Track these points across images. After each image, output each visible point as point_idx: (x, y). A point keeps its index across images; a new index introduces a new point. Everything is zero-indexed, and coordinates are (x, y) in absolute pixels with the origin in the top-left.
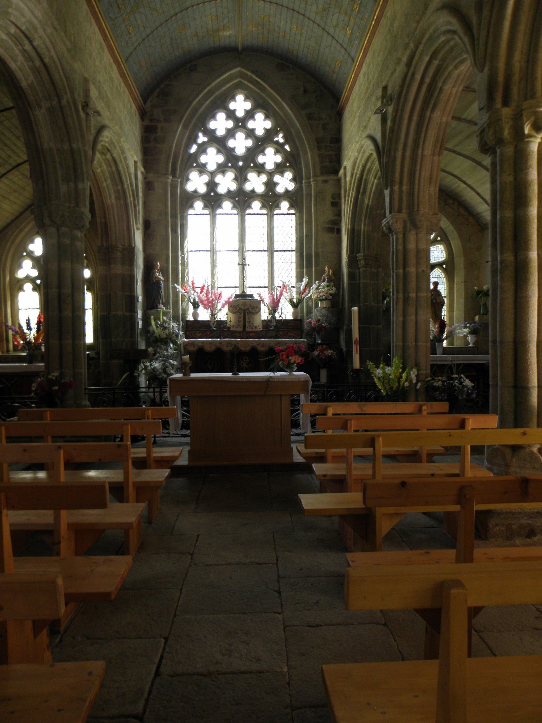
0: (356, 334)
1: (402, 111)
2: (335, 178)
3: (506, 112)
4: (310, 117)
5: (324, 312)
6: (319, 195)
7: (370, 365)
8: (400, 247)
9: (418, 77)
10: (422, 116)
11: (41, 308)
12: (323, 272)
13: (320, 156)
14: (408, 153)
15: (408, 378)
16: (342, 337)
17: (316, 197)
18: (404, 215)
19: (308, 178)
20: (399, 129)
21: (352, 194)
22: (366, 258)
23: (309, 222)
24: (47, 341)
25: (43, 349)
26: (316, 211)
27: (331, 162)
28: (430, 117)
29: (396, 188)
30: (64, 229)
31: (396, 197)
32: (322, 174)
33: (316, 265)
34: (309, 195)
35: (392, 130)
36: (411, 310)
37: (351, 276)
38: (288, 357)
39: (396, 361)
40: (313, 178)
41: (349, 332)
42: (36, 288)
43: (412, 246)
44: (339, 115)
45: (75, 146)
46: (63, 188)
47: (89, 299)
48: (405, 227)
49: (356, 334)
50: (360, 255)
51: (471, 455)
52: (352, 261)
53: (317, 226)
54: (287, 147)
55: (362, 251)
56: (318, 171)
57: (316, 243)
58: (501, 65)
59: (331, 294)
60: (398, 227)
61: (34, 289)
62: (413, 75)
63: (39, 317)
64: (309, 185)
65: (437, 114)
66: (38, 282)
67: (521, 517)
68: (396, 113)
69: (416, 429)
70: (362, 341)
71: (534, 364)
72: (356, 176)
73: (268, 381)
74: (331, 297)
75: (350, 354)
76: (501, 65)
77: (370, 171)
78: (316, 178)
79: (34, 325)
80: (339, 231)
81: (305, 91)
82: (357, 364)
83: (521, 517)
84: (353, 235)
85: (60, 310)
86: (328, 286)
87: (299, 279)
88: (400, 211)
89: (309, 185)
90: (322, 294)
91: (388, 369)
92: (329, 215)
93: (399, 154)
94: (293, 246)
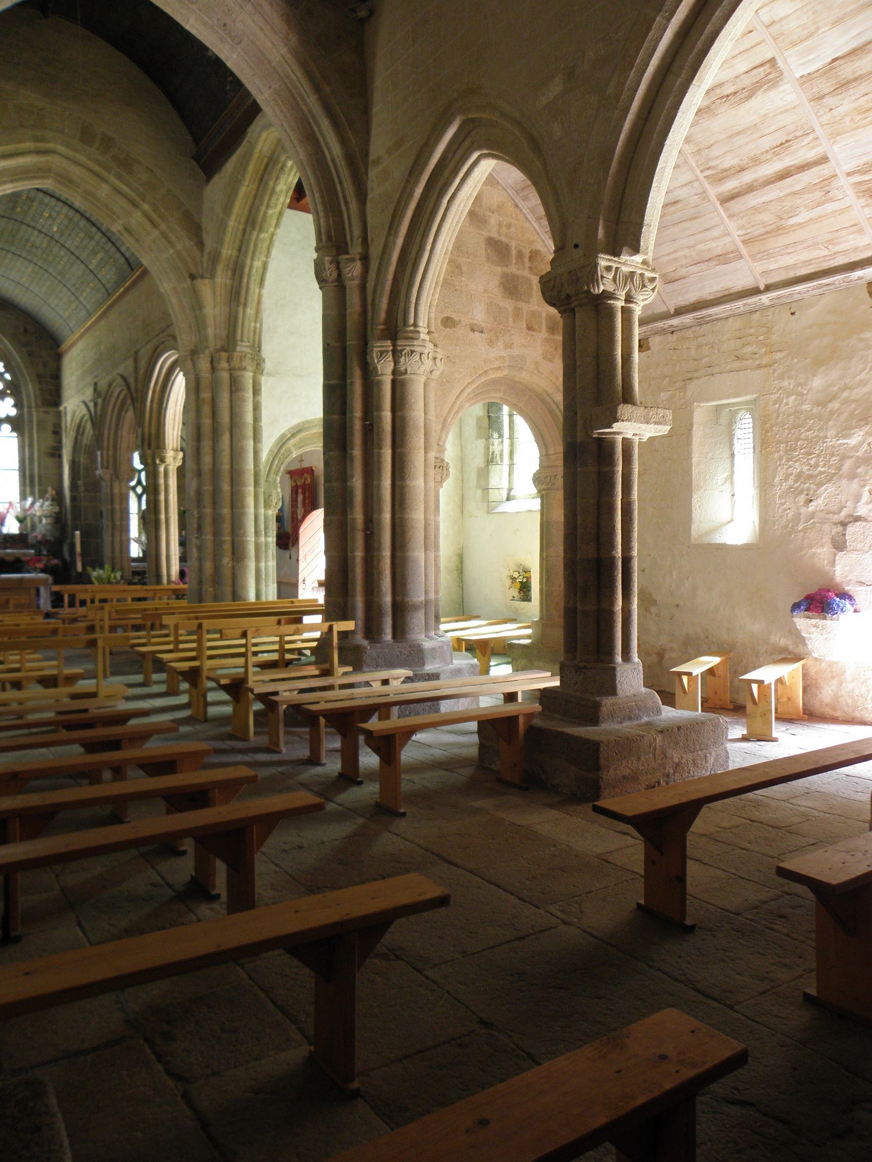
0: (78, 548)
2: (56, 410)
3: (149, 452)
4: (30, 354)
5: (49, 527)
6: (41, 424)
7: (89, 569)
8: (109, 491)
9: (115, 395)
10: (119, 415)
12: (46, 492)
13: (41, 390)
14: (112, 432)
15: (115, 578)
16: (66, 549)
17: (38, 425)
18: (110, 471)
19: (29, 407)
21: (72, 434)
22: (85, 485)
23: (31, 446)
26: (38, 437)
29: (105, 452)
31: (105, 458)
32: (43, 405)
33: (40, 485)
34: (31, 422)
35: (101, 416)
36: (117, 533)
37: (73, 499)
38: (34, 564)
39: (107, 566)
41: (72, 546)
43: (116, 491)
44: (59, 357)
48: (111, 479)
49: (78, 548)
50: (80, 483)
52: (74, 486)
53: (39, 450)
54: (8, 376)
55: (82, 478)
57: (39, 466)
58: (146, 430)
59: (55, 513)
60: (107, 477)
62: (112, 392)
64: (30, 413)
70: (84, 554)
73: (21, 580)
74: (55, 515)
75: (73, 563)
76: (146, 430)
80: (60, 457)
81: (25, 331)
82: (79, 568)
84: (74, 465)
86: (52, 505)
87: (23, 497)
88: (107, 468)
89: (30, 413)
90: (46, 512)
91: (101, 572)
92: (50, 441)
93: (106, 432)
94: (17, 468)
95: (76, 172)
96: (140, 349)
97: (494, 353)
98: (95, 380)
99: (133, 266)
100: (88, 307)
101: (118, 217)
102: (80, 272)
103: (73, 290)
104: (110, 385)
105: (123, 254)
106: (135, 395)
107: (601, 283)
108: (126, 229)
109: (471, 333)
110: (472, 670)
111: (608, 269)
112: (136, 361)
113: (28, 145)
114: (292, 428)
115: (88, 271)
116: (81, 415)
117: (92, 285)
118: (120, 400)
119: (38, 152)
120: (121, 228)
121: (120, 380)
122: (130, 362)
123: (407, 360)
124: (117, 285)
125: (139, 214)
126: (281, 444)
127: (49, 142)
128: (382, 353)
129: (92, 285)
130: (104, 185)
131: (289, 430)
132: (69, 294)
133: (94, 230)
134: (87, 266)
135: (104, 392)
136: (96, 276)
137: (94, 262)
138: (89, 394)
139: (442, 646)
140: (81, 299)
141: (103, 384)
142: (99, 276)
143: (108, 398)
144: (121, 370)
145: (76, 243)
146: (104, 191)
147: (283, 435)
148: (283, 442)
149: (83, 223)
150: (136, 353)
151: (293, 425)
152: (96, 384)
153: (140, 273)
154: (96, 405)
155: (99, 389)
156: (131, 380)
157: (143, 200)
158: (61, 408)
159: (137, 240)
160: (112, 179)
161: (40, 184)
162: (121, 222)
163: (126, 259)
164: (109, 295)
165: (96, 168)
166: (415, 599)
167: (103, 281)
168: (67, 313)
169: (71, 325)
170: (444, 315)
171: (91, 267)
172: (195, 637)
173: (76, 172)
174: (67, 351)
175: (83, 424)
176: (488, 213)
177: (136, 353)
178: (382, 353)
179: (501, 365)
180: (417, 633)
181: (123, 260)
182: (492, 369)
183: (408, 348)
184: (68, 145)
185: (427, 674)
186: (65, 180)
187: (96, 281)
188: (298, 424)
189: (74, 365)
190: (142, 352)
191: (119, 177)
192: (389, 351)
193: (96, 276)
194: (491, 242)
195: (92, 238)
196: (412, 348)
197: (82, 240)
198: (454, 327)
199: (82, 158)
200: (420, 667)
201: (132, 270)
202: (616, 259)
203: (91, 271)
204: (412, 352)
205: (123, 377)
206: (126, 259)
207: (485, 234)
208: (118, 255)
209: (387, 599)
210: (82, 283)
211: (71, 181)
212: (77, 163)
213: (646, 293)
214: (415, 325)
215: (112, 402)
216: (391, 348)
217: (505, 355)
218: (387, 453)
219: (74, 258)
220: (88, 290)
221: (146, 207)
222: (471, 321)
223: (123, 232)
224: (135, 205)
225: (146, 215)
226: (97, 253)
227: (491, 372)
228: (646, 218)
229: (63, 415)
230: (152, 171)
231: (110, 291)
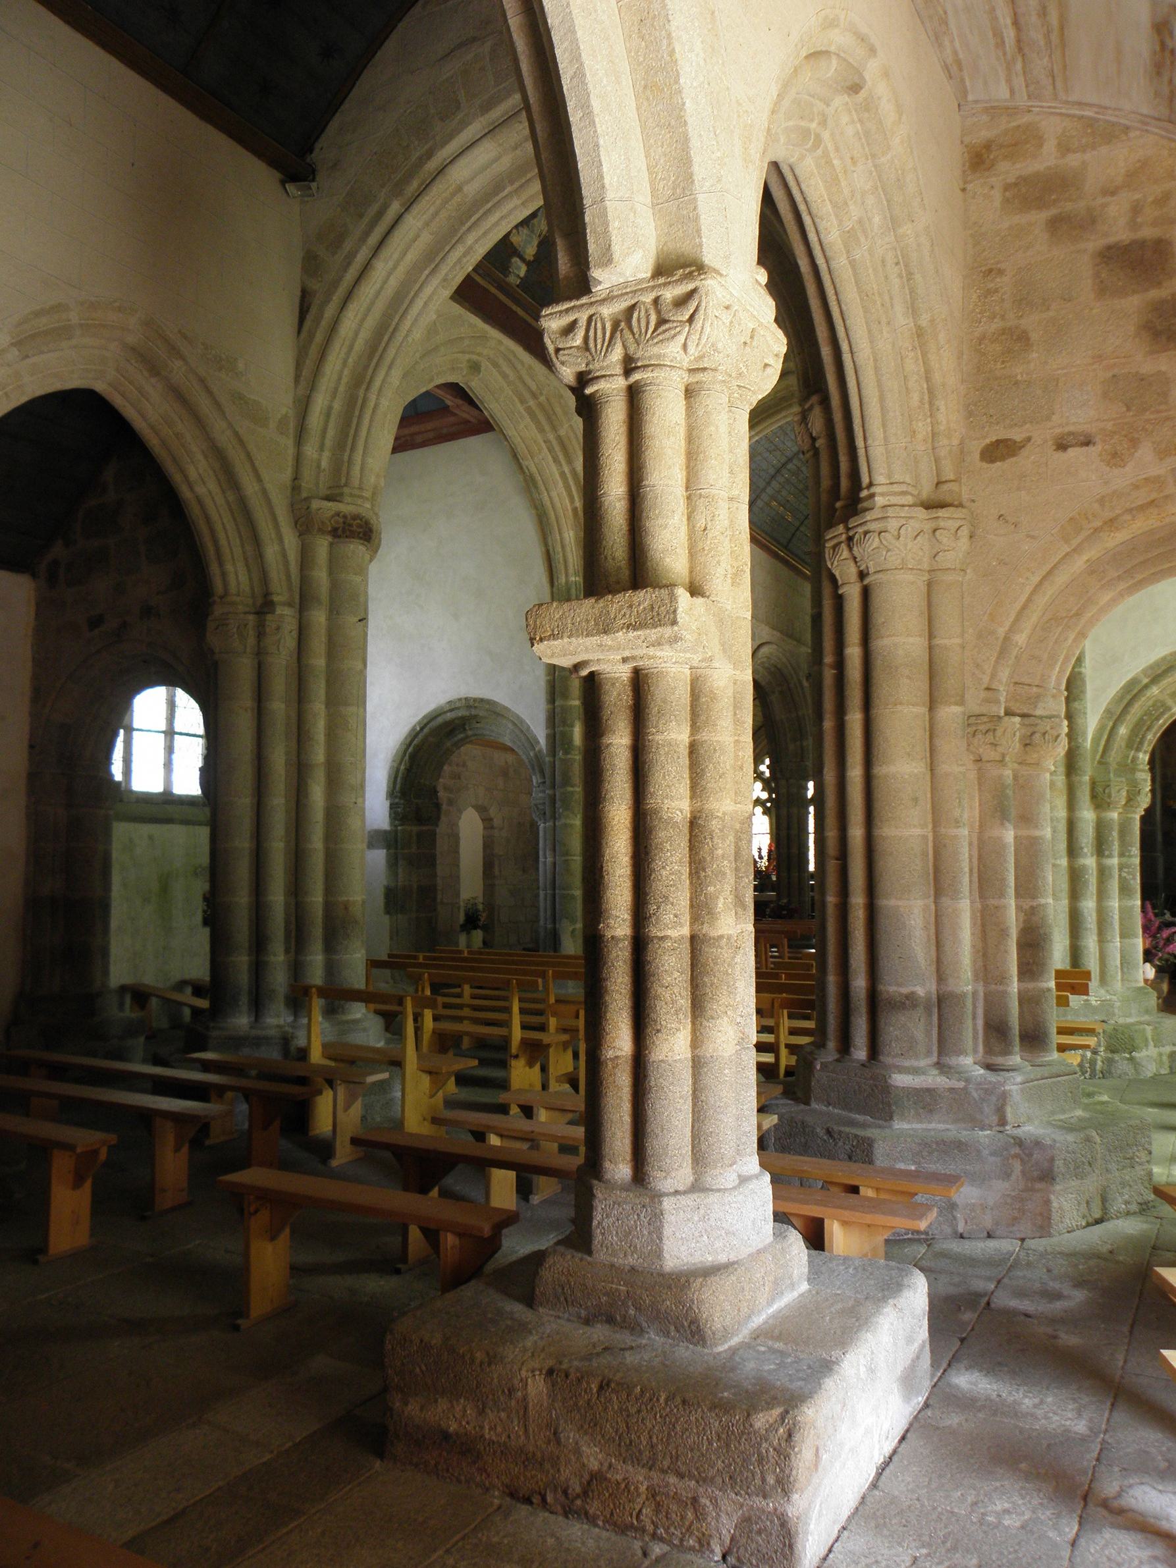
11: (771, 833)
24: (778, 869)
25: (774, 878)
30: (791, 781)
42: (766, 812)
45: (800, 713)
46: (791, 747)
47: (811, 809)
51: (1019, 980)
61: (764, 813)
63: (770, 846)
66: (769, 805)
71: (1136, 892)
79: (765, 853)
85: (789, 848)
97: (1122, 478)
107: (558, 365)
109: (1061, 455)
110: (1017, 1150)
111: (570, 328)
114: (1151, 667)
123: (861, 551)
126: (1129, 697)
128: (834, 547)
131: (1144, 671)
139: (965, 1089)
147: (1133, 682)
148: (1132, 692)
151: (1151, 661)
166: (892, 989)
170: (988, 441)
172: (810, 1024)
176: (1100, 200)
178: (834, 547)
179: (1154, 495)
180: (894, 1057)
182: (1130, 511)
183: (860, 530)
185: (856, 1136)
188: (1164, 659)
192: (840, 543)
194: (1113, 256)
196: (865, 528)
198: (1014, 455)
200: (886, 1120)
202: (584, 300)
204: (866, 533)
207: (1094, 243)
209: (859, 983)
213: (667, 335)
214: (871, 485)
216: (844, 536)
217: (1162, 472)
218: (855, 718)
222: (1058, 431)
227: (1128, 517)
228: (585, 192)
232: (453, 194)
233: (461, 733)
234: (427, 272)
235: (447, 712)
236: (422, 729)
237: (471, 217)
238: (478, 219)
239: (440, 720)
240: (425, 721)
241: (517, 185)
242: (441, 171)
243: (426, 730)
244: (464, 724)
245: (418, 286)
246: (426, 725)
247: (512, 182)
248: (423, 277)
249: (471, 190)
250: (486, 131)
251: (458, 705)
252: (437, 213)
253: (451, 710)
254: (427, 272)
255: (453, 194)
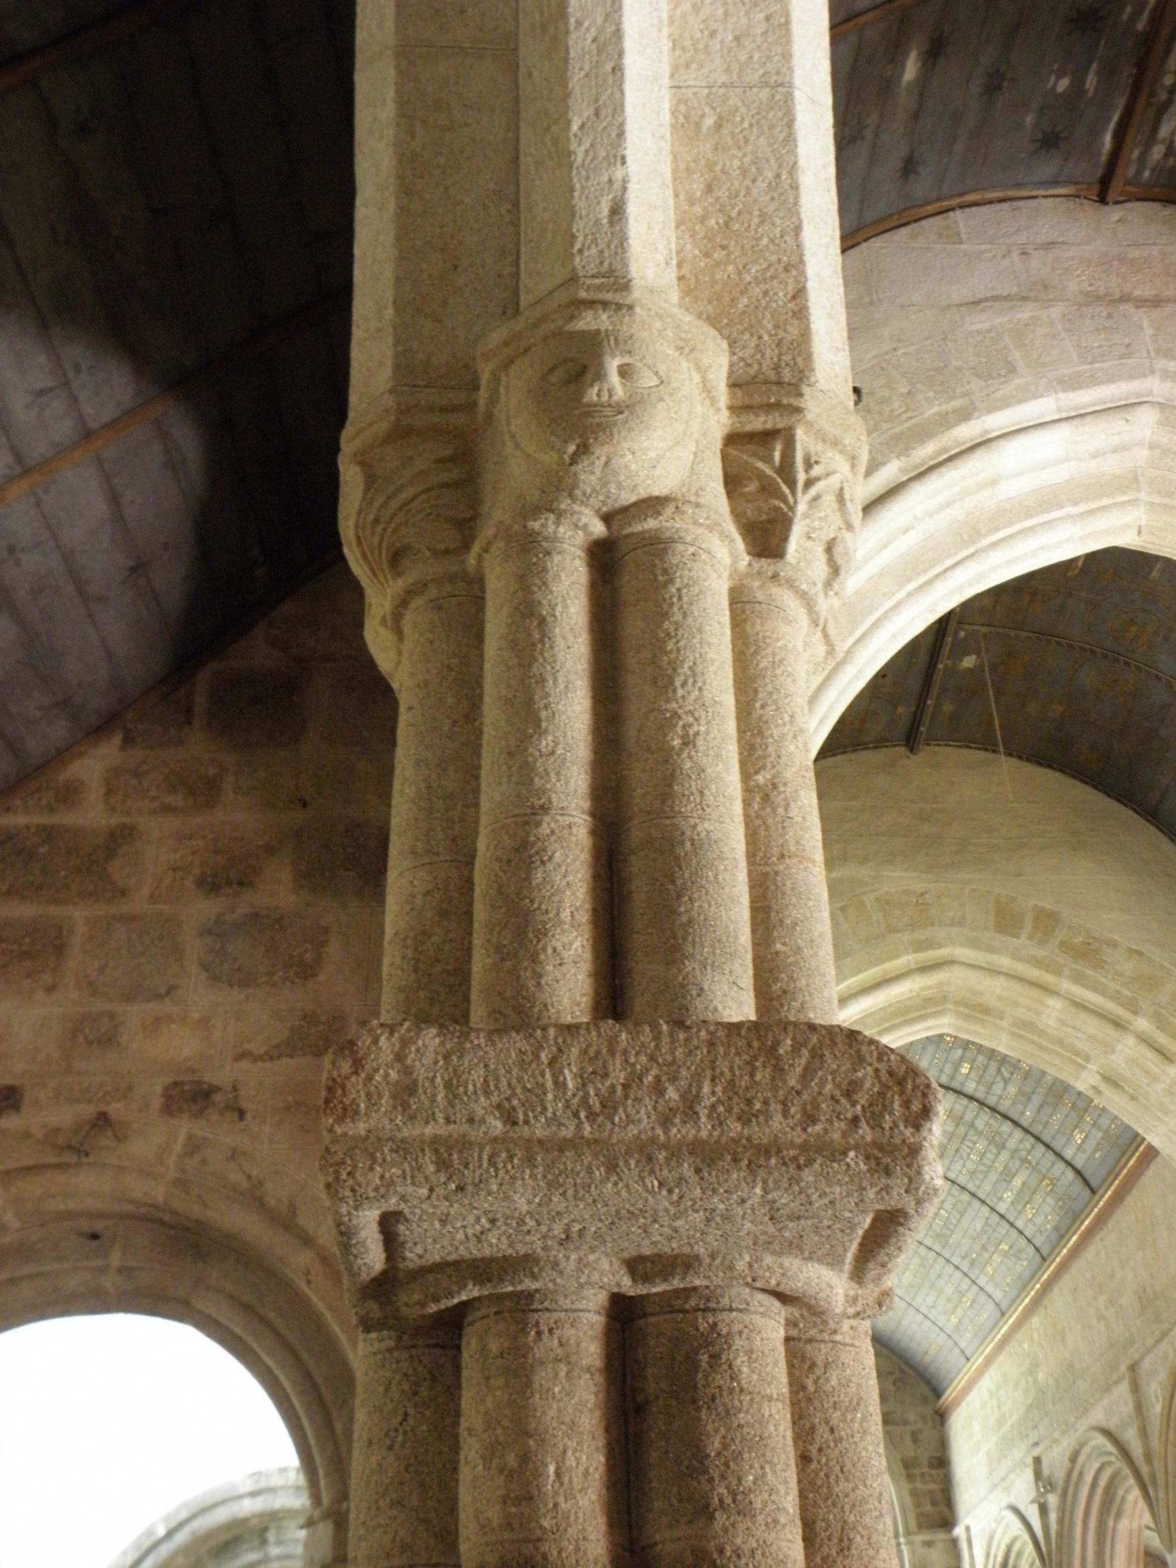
1: (1072, 1513)
9: (1088, 1479)
10: (1102, 1524)
13: (914, 1493)
20: (1071, 1537)
27: (934, 1503)
28: (1114, 1529)
32: (921, 1527)
35: (1060, 1534)
40: (905, 1536)
44: (941, 1417)
56: (913, 1524)
62: (1081, 1474)
65: (1124, 1525)
67: (559, 1553)
68: (1063, 1514)
69: (967, 210)
72: (995, 1557)
77: (1019, 1554)
78: (910, 1538)
83: (559, 1553)
95: (993, 989)
96: (1142, 1359)
98: (1036, 1452)
99: (1094, 1182)
100: (998, 1295)
101: (1088, 1059)
102: (979, 1225)
103: (965, 1267)
104: (1074, 1459)
105: (1069, 1164)
106: (1145, 1470)
108: (1107, 1079)
112: (1135, 1387)
113: (907, 960)
115: (996, 1218)
116: (1007, 1540)
117: (1004, 1247)
118: (1099, 1492)
119: (925, 968)
120: (1095, 1080)
121: (1100, 1440)
122: (1123, 1390)
124: (1062, 1234)
125: (1131, 1041)
127: (940, 947)
129: (1004, 1247)
130: (1051, 1001)
132: (958, 1274)
133: (1007, 1127)
134: (992, 1209)
135: (1060, 1475)
136: (1012, 1225)
137: (1009, 1196)
138: (1023, 1489)
140: (982, 1281)
141: (1056, 1458)
142: (1019, 1224)
143: (1071, 1490)
144: (1098, 1415)
145: (970, 1166)
146: (1053, 1012)
149: (984, 1119)
150: (1133, 1368)
152: (1037, 1461)
153: (1113, 1193)
154: (1043, 1509)
155: (1046, 1472)
156: (1131, 1436)
157: (1135, 1013)
158: (959, 1531)
159: (1133, 1098)
160: (1066, 985)
161: (930, 1028)
162: (1093, 1067)
163: (1078, 1172)
164: (1044, 1259)
165: (1034, 973)
167: (1028, 1232)
168: (954, 1319)
169: (963, 1344)
171: (1002, 1208)
173: (993, 989)
174: (957, 1402)
175: (1011, 1562)
177: (1133, 1368)
181: (1070, 1174)
184: (975, 944)
186: (976, 1009)
187: (1015, 1234)
189: (977, 1427)
190: (1147, 1363)
191: (1079, 979)
193: (1012, 1225)
195: (1002, 1147)
197: (982, 1156)
199: (1004, 962)
201: (1093, 1192)
203: (1002, 1216)
205: (1107, 1433)
206: (1078, 1172)
208: (1060, 1166)
210: (984, 1248)
211: (987, 1011)
212: (994, 972)
215: (1085, 1491)
219: (966, 1197)
220: (997, 1258)
221: (1142, 1024)
223: (1104, 1087)
224: (1118, 1025)
225: (1144, 1039)
226: (1014, 1176)
229: (964, 1546)
230: (1140, 953)
231: (1045, 1252)
232: (981, 487)
233: (252, 1549)
234: (911, 587)
235: (241, 1497)
236: (169, 1534)
237: (997, 529)
238: (1010, 537)
239: (222, 1515)
240: (184, 1515)
241: (1083, 508)
242: (984, 443)
243: (181, 1537)
244: (265, 1530)
245: (889, 604)
246: (180, 1526)
247: (1075, 504)
248: (901, 594)
249: (1011, 489)
250: (1064, 415)
251: (276, 1481)
252: (948, 505)
253: (254, 1494)
254: (911, 587)
255: (981, 487)
